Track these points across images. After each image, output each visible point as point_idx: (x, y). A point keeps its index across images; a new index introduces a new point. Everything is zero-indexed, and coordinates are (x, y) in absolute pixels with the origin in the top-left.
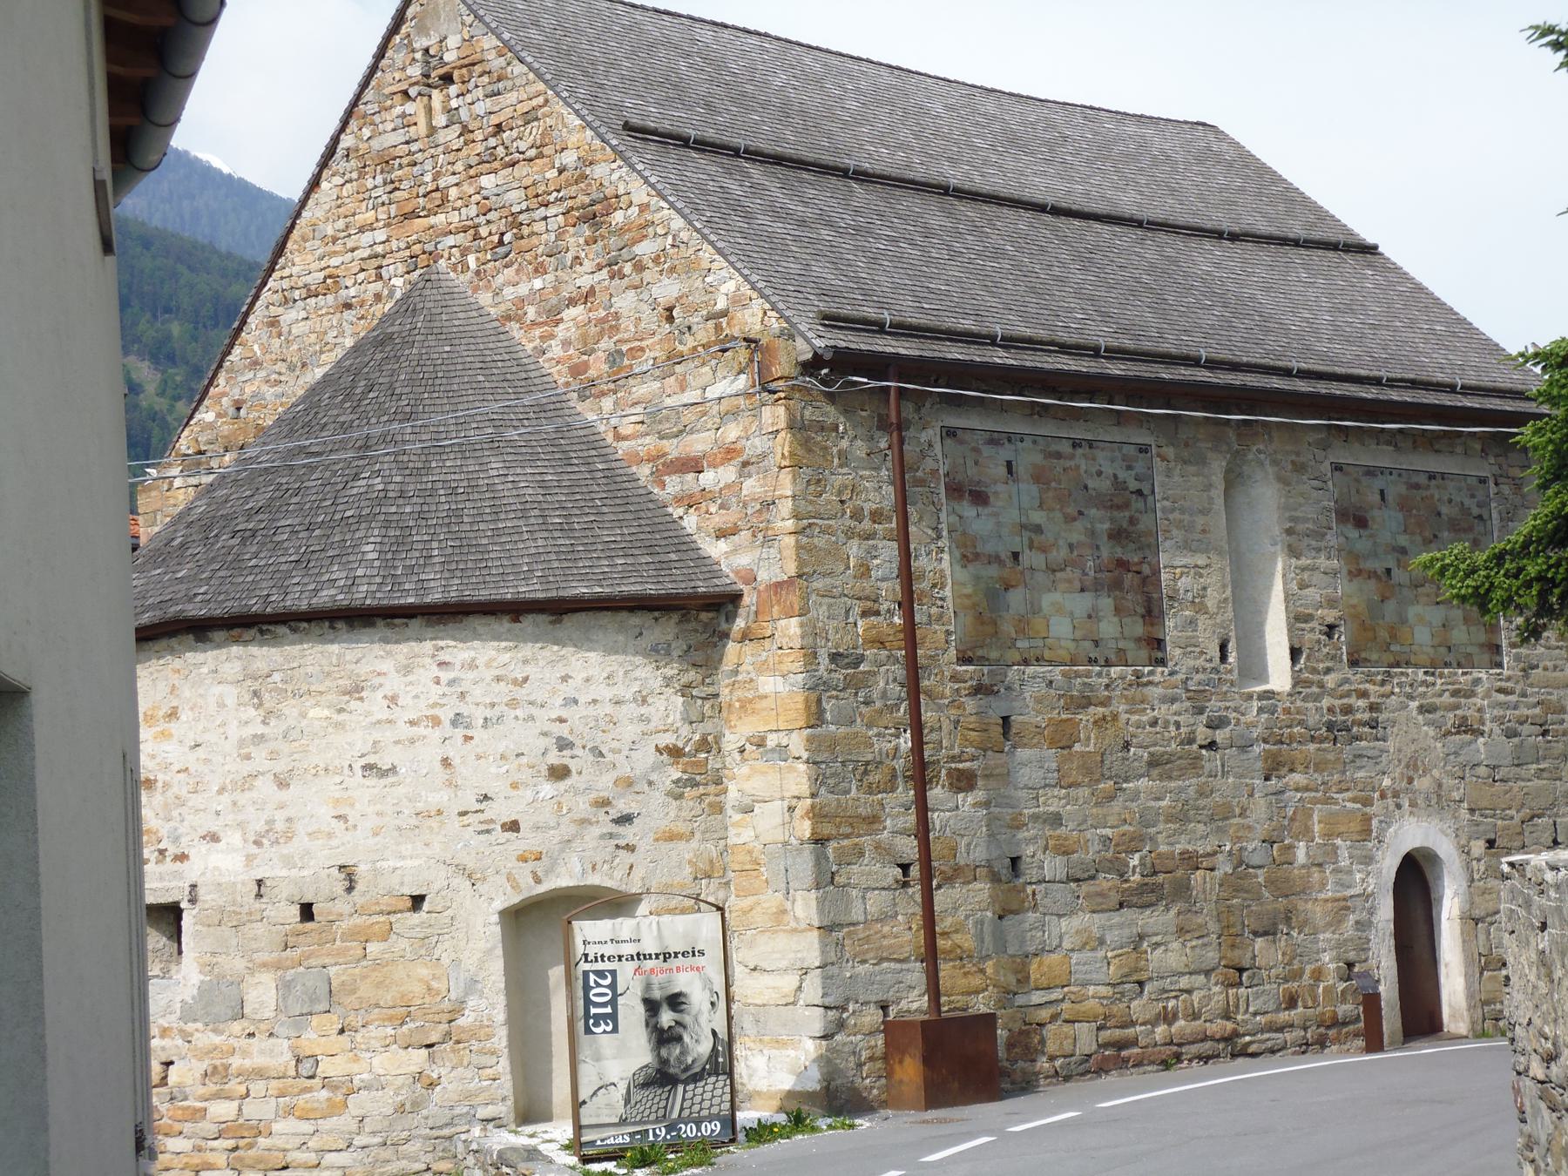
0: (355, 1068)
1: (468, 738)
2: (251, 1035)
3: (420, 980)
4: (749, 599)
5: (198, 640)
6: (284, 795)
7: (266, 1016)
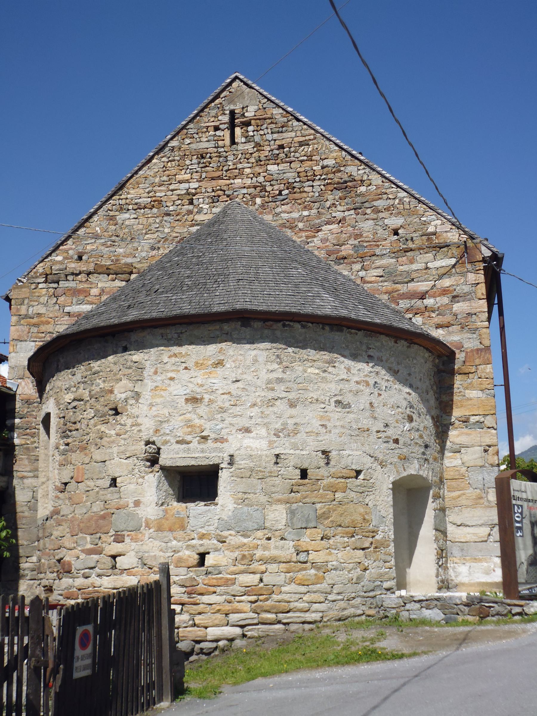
0: (330, 558)
1: (380, 395)
2: (269, 539)
3: (360, 514)
4: (460, 356)
5: (243, 325)
6: (293, 411)
7: (280, 527)
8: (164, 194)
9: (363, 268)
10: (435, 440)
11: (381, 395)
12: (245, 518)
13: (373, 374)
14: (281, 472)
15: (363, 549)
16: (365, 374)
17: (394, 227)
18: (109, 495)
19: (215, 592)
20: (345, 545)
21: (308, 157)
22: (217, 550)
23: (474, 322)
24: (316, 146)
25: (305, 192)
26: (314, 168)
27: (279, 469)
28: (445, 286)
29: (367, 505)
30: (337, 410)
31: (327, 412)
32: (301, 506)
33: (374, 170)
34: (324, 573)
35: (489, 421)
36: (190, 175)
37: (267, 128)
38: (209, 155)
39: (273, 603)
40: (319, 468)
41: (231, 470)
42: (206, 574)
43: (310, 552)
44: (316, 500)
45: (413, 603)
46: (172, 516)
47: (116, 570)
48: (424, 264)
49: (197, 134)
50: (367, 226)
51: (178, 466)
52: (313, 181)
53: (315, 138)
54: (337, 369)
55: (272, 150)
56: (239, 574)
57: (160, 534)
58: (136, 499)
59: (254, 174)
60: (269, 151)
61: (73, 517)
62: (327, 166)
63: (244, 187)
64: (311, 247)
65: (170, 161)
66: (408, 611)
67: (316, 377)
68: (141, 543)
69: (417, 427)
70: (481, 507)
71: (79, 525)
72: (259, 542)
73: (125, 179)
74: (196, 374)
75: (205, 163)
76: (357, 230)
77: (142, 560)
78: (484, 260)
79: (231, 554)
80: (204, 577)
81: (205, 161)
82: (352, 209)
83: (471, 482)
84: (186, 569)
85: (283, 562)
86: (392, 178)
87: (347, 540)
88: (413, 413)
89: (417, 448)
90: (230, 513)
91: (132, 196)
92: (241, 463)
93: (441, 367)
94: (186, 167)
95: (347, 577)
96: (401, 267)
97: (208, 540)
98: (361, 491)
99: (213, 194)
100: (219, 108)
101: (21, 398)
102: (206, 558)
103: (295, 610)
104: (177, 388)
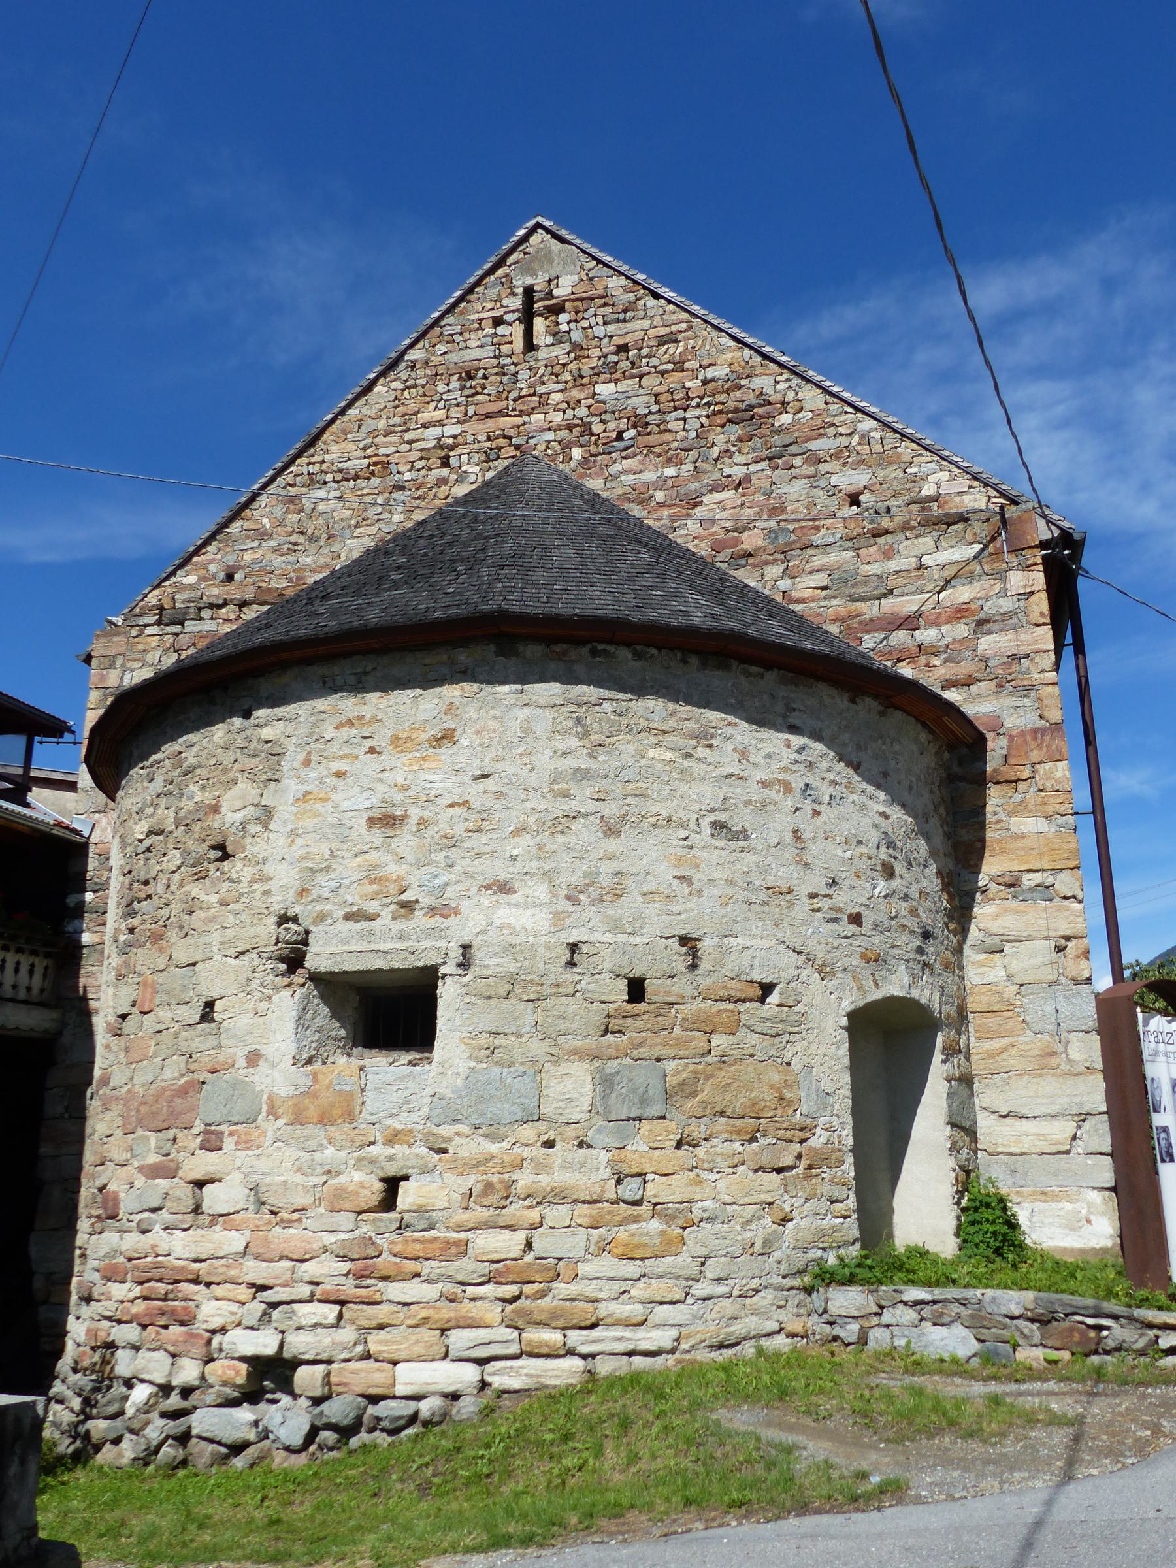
1: (816, 813)
2: (550, 1144)
3: (772, 1087)
4: (996, 746)
5: (501, 652)
6: (612, 845)
7: (576, 1117)
8: (394, 449)
9: (786, 573)
10: (946, 924)
11: (819, 814)
12: (493, 1092)
13: (801, 767)
14: (583, 985)
15: (779, 1171)
16: (782, 765)
17: (851, 489)
18: (198, 1040)
19: (417, 1275)
20: (736, 1161)
21: (675, 364)
22: (425, 1171)
23: (1025, 673)
24: (691, 342)
25: (670, 431)
26: (688, 384)
27: (578, 978)
28: (961, 601)
29: (788, 1064)
30: (716, 843)
31: (692, 847)
32: (630, 1066)
33: (808, 381)
34: (684, 1228)
35: (1066, 883)
36: (444, 411)
37: (595, 315)
38: (481, 373)
39: (556, 1303)
40: (673, 977)
41: (465, 980)
42: (399, 1228)
43: (649, 1177)
44: (665, 1052)
45: (900, 1306)
46: (328, 1088)
47: (201, 1217)
48: (914, 560)
49: (461, 334)
50: (794, 491)
51: (345, 972)
52: (685, 410)
53: (689, 328)
54: (716, 752)
55: (605, 356)
56: (477, 1229)
57: (299, 1130)
58: (253, 1047)
59: (568, 403)
60: (600, 358)
61: (129, 1091)
62: (713, 380)
63: (550, 429)
64: (681, 536)
65: (408, 388)
66: (888, 1326)
67: (668, 768)
68: (257, 1152)
69: (905, 890)
70: (1053, 1075)
71: (138, 1111)
72: (526, 1153)
73: (321, 425)
74: (393, 763)
75: (475, 388)
76: (774, 499)
77: (257, 1193)
78: (1043, 545)
79: (460, 1180)
80: (394, 1236)
81: (474, 383)
82: (764, 460)
83: (1028, 1018)
84: (353, 1215)
85: (584, 1202)
86: (845, 394)
87: (741, 1149)
88: (896, 858)
89: (904, 938)
90: (459, 1082)
91: (334, 456)
92: (487, 962)
93: (956, 769)
94: (438, 397)
95: (739, 1238)
96: (866, 567)
97: (405, 1147)
98: (773, 1032)
99: (488, 444)
100: (503, 284)
101: (97, 851)
102: (400, 1191)
103: (609, 1320)
104: (351, 794)
